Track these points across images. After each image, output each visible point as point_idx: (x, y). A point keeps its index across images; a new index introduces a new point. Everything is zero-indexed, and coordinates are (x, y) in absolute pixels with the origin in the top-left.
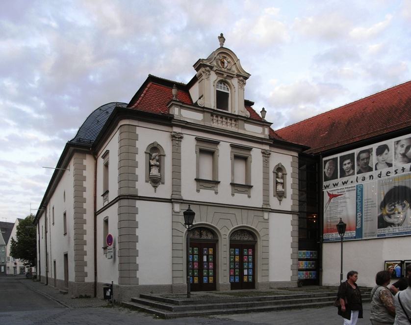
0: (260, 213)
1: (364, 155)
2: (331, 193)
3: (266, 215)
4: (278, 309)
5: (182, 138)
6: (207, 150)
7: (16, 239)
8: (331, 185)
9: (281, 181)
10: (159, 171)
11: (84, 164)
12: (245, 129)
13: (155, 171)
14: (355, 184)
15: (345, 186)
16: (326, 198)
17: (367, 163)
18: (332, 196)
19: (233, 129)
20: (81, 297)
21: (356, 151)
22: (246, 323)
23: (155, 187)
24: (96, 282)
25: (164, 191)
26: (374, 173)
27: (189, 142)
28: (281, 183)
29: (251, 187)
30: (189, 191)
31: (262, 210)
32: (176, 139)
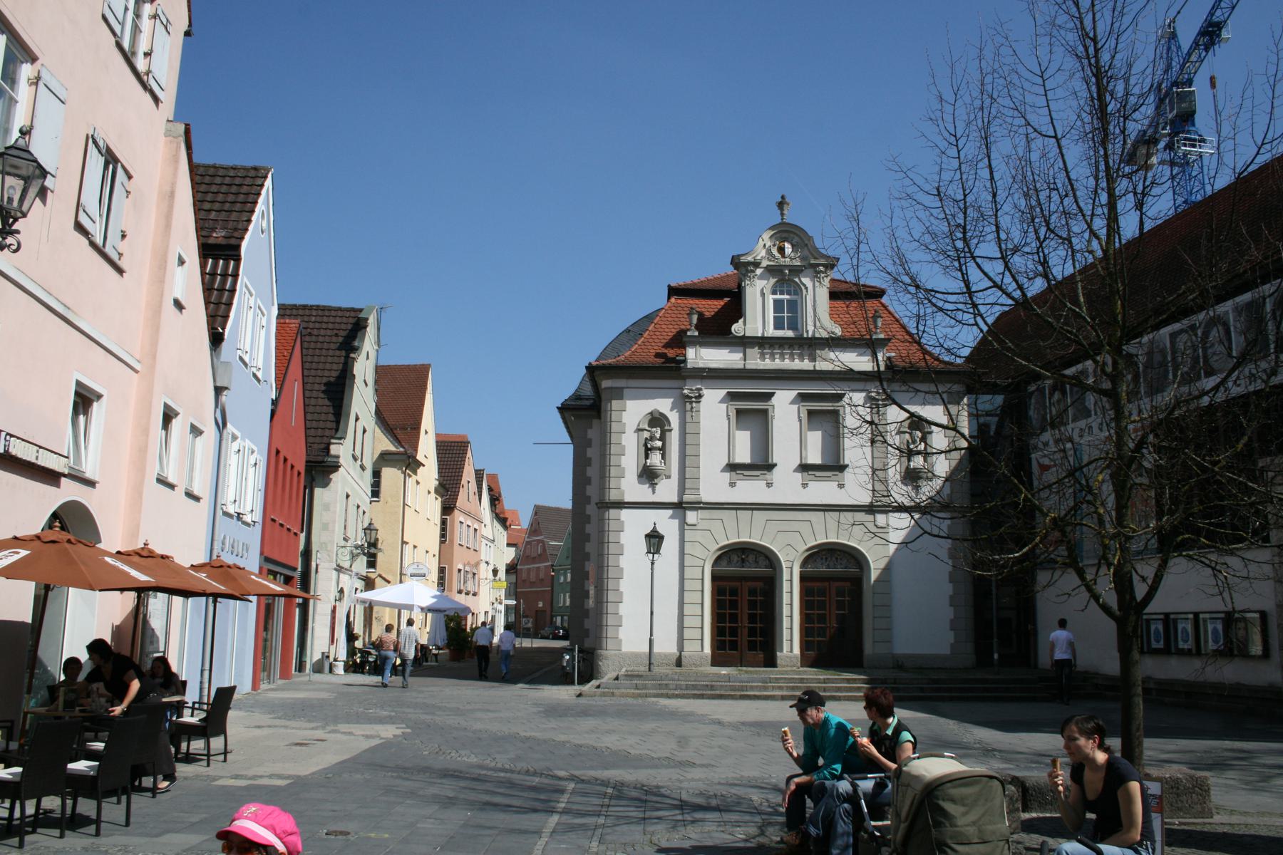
0: (861, 516)
2: (1238, 343)
3: (881, 519)
5: (700, 396)
6: (752, 414)
10: (663, 457)
13: (655, 459)
19: (806, 365)
20: (297, 744)
23: (653, 486)
25: (667, 490)
27: (713, 402)
30: (714, 485)
31: (871, 509)
32: (687, 403)
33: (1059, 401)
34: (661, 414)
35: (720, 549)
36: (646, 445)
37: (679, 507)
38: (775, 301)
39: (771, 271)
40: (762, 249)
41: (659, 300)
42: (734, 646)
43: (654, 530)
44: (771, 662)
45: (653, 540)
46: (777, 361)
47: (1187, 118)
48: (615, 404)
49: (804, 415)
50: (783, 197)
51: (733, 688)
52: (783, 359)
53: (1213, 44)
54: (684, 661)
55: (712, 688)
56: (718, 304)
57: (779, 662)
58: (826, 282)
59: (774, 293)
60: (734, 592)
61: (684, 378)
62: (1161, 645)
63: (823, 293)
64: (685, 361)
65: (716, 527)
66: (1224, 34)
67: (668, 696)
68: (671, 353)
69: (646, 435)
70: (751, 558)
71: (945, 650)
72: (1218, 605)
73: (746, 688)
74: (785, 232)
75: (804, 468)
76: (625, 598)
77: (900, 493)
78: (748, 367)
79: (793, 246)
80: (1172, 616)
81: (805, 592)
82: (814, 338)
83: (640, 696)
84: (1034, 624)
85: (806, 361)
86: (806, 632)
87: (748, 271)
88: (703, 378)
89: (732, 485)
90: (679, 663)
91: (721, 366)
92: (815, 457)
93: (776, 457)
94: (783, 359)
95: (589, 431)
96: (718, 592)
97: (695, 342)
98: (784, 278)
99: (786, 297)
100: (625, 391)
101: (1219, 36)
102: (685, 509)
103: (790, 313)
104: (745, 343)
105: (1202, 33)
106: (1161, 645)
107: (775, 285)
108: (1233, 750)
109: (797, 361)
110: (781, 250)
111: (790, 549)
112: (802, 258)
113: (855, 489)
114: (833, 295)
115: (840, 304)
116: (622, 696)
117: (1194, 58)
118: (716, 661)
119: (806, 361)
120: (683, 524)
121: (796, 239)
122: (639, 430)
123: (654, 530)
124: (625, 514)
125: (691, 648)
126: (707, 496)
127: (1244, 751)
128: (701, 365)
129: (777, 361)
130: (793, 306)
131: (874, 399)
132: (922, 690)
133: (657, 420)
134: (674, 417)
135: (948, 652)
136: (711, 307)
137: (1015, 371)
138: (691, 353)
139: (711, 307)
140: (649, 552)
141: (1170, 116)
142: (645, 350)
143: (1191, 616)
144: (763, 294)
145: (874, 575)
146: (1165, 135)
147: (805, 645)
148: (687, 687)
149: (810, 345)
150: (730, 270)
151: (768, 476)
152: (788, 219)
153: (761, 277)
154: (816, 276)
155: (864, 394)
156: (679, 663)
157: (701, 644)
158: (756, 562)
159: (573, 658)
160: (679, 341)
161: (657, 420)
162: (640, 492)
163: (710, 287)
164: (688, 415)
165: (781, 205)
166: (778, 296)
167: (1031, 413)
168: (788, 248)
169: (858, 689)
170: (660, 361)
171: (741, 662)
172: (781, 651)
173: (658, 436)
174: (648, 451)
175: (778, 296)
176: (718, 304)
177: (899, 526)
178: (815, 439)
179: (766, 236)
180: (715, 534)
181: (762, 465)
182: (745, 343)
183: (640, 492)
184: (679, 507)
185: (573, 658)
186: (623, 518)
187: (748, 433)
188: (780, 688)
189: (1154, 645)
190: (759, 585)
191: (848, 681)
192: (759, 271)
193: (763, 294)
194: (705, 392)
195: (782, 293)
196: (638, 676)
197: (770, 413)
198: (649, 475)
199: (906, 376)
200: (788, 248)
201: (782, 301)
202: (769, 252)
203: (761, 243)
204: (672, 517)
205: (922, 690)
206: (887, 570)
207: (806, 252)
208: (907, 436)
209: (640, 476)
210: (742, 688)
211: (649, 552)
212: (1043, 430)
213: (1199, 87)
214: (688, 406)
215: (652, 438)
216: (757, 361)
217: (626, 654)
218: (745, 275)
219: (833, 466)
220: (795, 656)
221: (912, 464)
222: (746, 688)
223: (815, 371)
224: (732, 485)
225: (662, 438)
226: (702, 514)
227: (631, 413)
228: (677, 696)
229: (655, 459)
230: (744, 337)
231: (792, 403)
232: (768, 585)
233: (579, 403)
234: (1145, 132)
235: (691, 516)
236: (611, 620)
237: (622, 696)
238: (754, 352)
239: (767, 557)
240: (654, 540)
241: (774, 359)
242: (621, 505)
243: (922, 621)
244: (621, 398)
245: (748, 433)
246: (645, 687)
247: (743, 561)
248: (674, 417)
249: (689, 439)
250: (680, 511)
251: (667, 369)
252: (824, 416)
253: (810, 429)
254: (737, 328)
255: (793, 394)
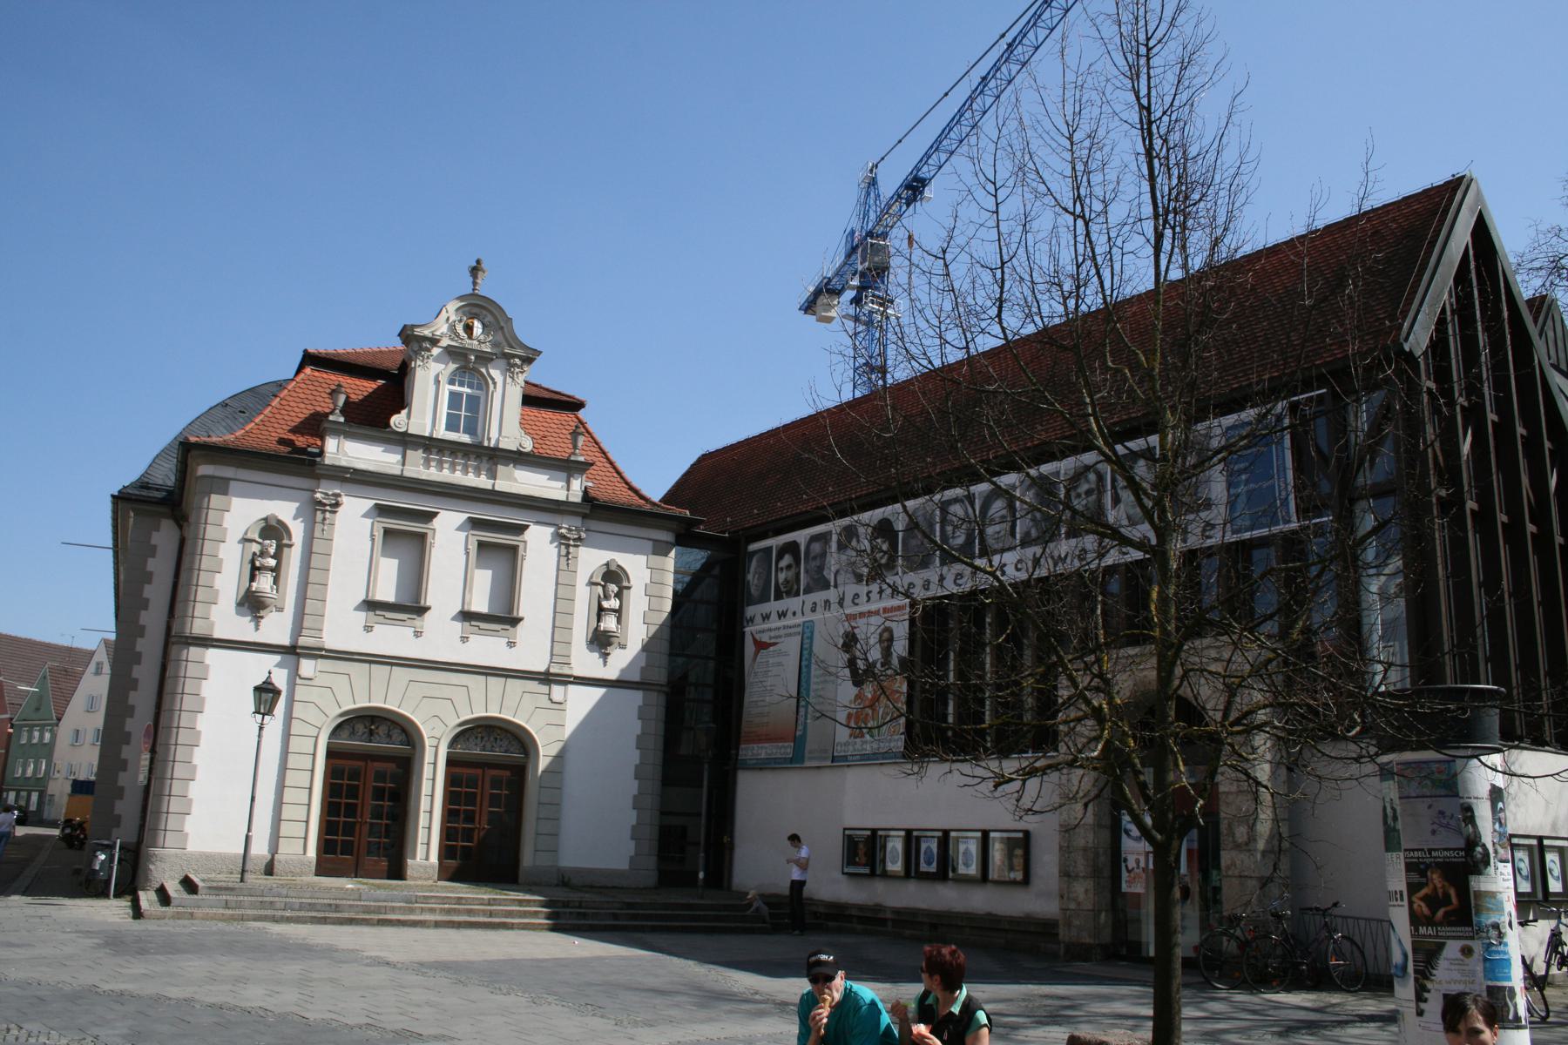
1: (816, 547)
3: (557, 691)
4: (437, 925)
5: (337, 505)
6: (405, 536)
7: (1496, 418)
8: (774, 616)
9: (613, 603)
10: (276, 581)
11: (153, 542)
12: (515, 480)
13: (264, 583)
14: (799, 620)
15: (784, 622)
16: (749, 648)
17: (821, 568)
18: (761, 646)
21: (801, 536)
22: (731, 1012)
23: (257, 619)
24: (272, 860)
25: (276, 628)
26: (832, 594)
28: (614, 611)
29: (516, 622)
31: (546, 678)
32: (318, 511)
33: (789, 567)
34: (280, 522)
35: (341, 715)
36: (253, 562)
37: (292, 652)
38: (452, 394)
39: (452, 353)
40: (443, 324)
41: (285, 367)
42: (347, 848)
43: (268, 682)
44: (397, 871)
45: (264, 696)
46: (446, 472)
47: (882, 270)
48: (215, 500)
49: (473, 547)
50: (478, 262)
51: (367, 910)
52: (453, 470)
53: (915, 200)
54: (277, 867)
55: (337, 908)
56: (370, 386)
57: (409, 872)
58: (521, 379)
59: (452, 382)
60: (355, 775)
61: (318, 477)
62: (933, 868)
63: (515, 394)
64: (321, 453)
65: (341, 684)
66: (927, 193)
67: (275, 920)
68: (301, 441)
69: (256, 548)
70: (382, 730)
71: (624, 865)
72: (1008, 822)
73: (386, 910)
74: (478, 307)
75: (466, 616)
76: (199, 775)
77: (585, 662)
78: (406, 474)
79: (484, 326)
80: (953, 834)
81: (451, 780)
82: (496, 449)
83: (233, 918)
84: (732, 836)
85: (483, 477)
86: (448, 834)
87: (422, 349)
88: (344, 480)
89: (368, 629)
90: (269, 870)
91: (371, 468)
92: (480, 605)
93: (430, 599)
94: (466, 472)
95: (155, 534)
96: (332, 773)
97: (338, 431)
98: (467, 364)
99: (466, 390)
100: (232, 483)
101: (921, 193)
102: (298, 655)
103: (470, 411)
104: (406, 441)
105: (908, 187)
106: (933, 868)
107: (454, 373)
108: (1046, 996)
109: (471, 475)
110: (469, 329)
111: (437, 720)
112: (495, 344)
113: (529, 648)
114: (529, 400)
115: (533, 412)
116: (206, 918)
117: (895, 208)
118: (322, 869)
119: (483, 477)
120: (295, 675)
121: (489, 318)
122: (246, 540)
123: (268, 682)
124: (212, 655)
125: (288, 849)
126: (331, 641)
127: (1063, 998)
128: (344, 464)
129: (446, 472)
130: (474, 402)
131: (564, 537)
132: (616, 917)
133: (273, 530)
134: (297, 529)
135: (626, 867)
136: (361, 388)
137: (734, 520)
138: (331, 444)
139: (361, 388)
140: (257, 712)
141: (860, 268)
142: (265, 430)
143: (979, 834)
144: (437, 382)
145: (543, 763)
146: (853, 288)
147: (446, 852)
148: (301, 907)
149: (494, 457)
150: (399, 346)
151: (418, 622)
152: (481, 291)
153: (438, 360)
154: (509, 369)
155: (551, 530)
156: (269, 870)
157: (302, 842)
158: (389, 736)
159: (111, 859)
160: (316, 425)
161: (273, 530)
162: (242, 628)
163: (360, 361)
164: (318, 527)
165: (475, 271)
166: (457, 388)
167: (750, 577)
168: (478, 328)
169: (535, 914)
170: (284, 450)
171: (356, 871)
172: (414, 857)
173: (272, 551)
174: (255, 570)
175: (457, 388)
176: (370, 386)
177: (581, 702)
178: (483, 579)
179: (452, 307)
180: (327, 698)
181: (411, 606)
182: (406, 441)
183: (242, 628)
184: (292, 652)
185: (111, 859)
186: (207, 662)
187: (396, 562)
188: (432, 910)
189: (924, 867)
190: (391, 767)
191: (520, 902)
192: (436, 351)
193: (437, 382)
194: (345, 499)
195: (462, 384)
196: (227, 889)
197: (429, 539)
198: (252, 604)
199: (606, 514)
200: (478, 328)
201: (460, 395)
202: (452, 328)
203: (444, 315)
204: (279, 665)
205: (616, 917)
206: (560, 758)
207: (500, 337)
208: (600, 589)
209: (240, 604)
210: (378, 910)
211: (257, 712)
212: (764, 598)
213: (896, 240)
214: (319, 516)
215: (263, 554)
216: (418, 467)
217: (192, 854)
218: (417, 353)
219: (504, 617)
220: (432, 866)
221: (602, 626)
222: (386, 910)
223: (493, 492)
224: (368, 629)
225: (277, 556)
226: (323, 664)
227: (236, 516)
228: (289, 920)
229: (264, 583)
230: (405, 434)
231: (459, 529)
232: (404, 767)
233: (145, 493)
234: (830, 280)
235: (307, 667)
236: (175, 805)
237: (206, 918)
238: (416, 456)
239: (404, 731)
240: (266, 694)
241: (441, 469)
242: (207, 642)
243: (598, 824)
244: (225, 492)
245: (396, 562)
246: (239, 906)
247: (371, 733)
248: (297, 529)
249: (316, 561)
250: (291, 658)
251: (295, 461)
252: (499, 552)
253: (479, 566)
254: (398, 421)
255: (462, 517)
